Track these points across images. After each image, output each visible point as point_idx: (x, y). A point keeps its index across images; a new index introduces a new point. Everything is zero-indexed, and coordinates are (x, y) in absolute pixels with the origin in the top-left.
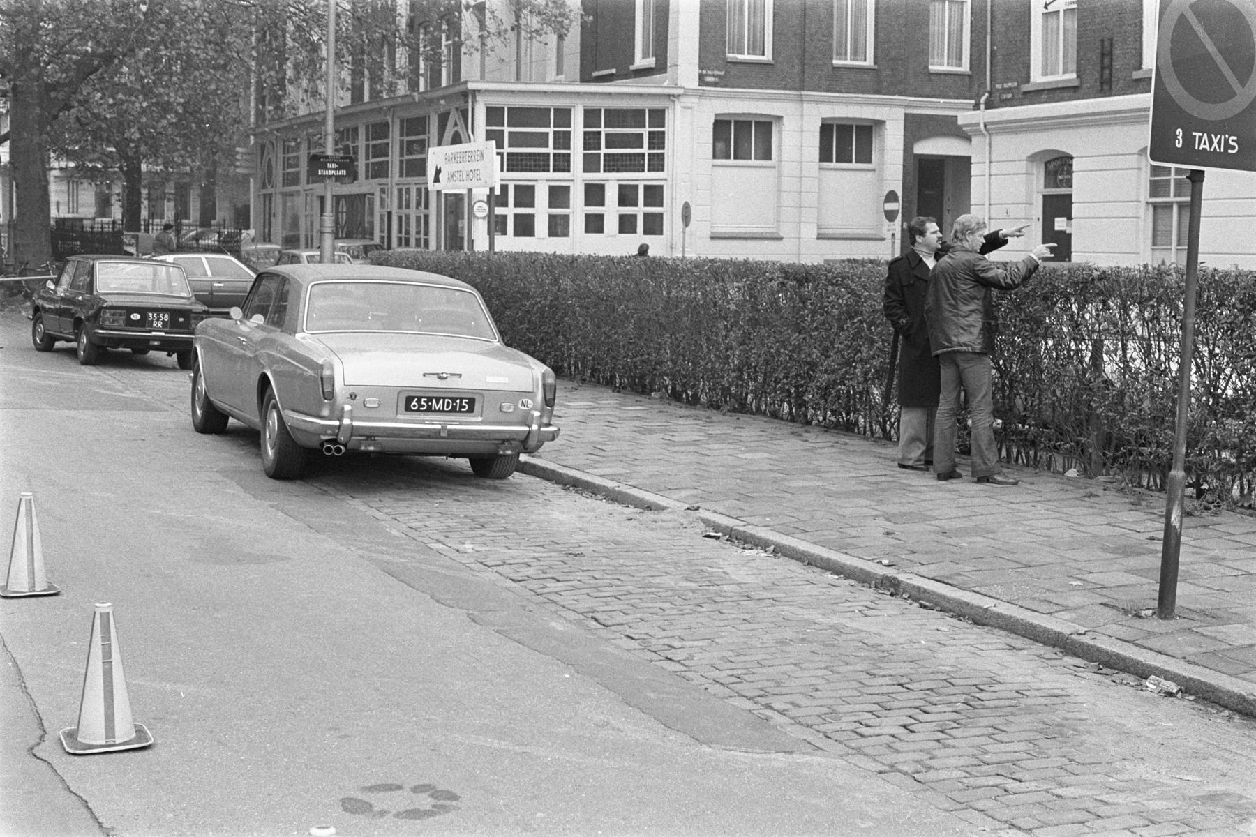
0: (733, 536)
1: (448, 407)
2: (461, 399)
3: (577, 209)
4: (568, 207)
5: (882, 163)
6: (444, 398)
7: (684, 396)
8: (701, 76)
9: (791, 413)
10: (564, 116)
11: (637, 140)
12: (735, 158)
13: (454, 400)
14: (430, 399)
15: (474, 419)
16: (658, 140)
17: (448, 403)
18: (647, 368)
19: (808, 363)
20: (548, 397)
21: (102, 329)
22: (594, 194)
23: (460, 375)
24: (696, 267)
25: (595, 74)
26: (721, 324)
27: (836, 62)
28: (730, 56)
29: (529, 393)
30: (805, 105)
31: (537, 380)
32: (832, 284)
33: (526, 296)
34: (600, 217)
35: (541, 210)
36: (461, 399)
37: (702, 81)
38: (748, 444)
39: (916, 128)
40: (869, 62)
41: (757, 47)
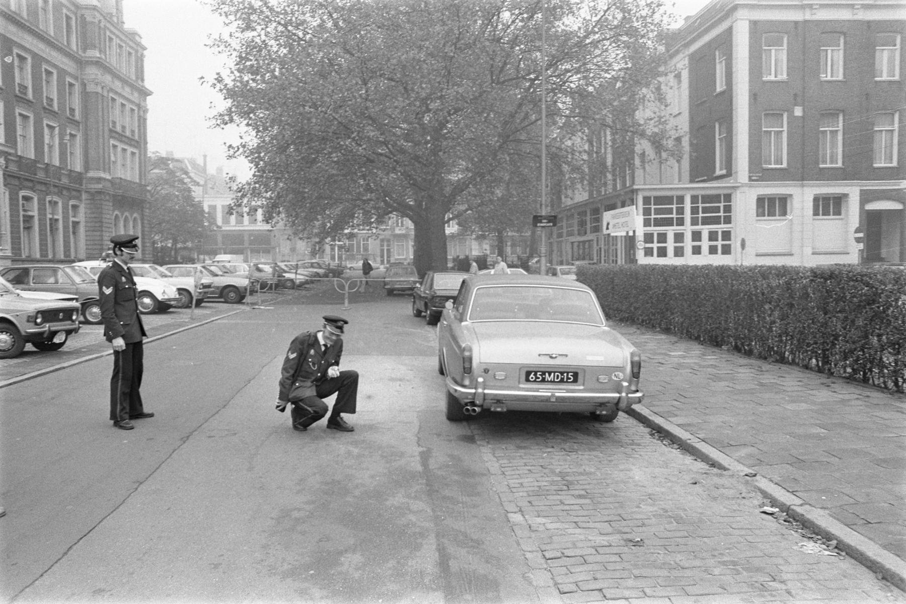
0: (792, 518)
1: (558, 378)
2: (568, 373)
3: (688, 244)
4: (683, 242)
5: (847, 215)
6: (555, 372)
7: (741, 349)
8: (750, 177)
9: (818, 365)
10: (681, 199)
11: (717, 210)
12: (768, 216)
13: (562, 373)
14: (544, 373)
15: (577, 388)
16: (728, 209)
17: (558, 376)
18: (719, 332)
19: (833, 335)
20: (635, 371)
21: (435, 307)
22: (697, 236)
23: (566, 356)
24: (750, 270)
25: (697, 180)
26: (767, 307)
27: (821, 166)
28: (764, 166)
29: (621, 369)
30: (805, 188)
31: (627, 359)
32: (853, 280)
33: (650, 288)
34: (699, 247)
35: (670, 245)
36: (568, 373)
37: (750, 179)
38: (789, 393)
39: (866, 197)
40: (840, 164)
41: (779, 161)
